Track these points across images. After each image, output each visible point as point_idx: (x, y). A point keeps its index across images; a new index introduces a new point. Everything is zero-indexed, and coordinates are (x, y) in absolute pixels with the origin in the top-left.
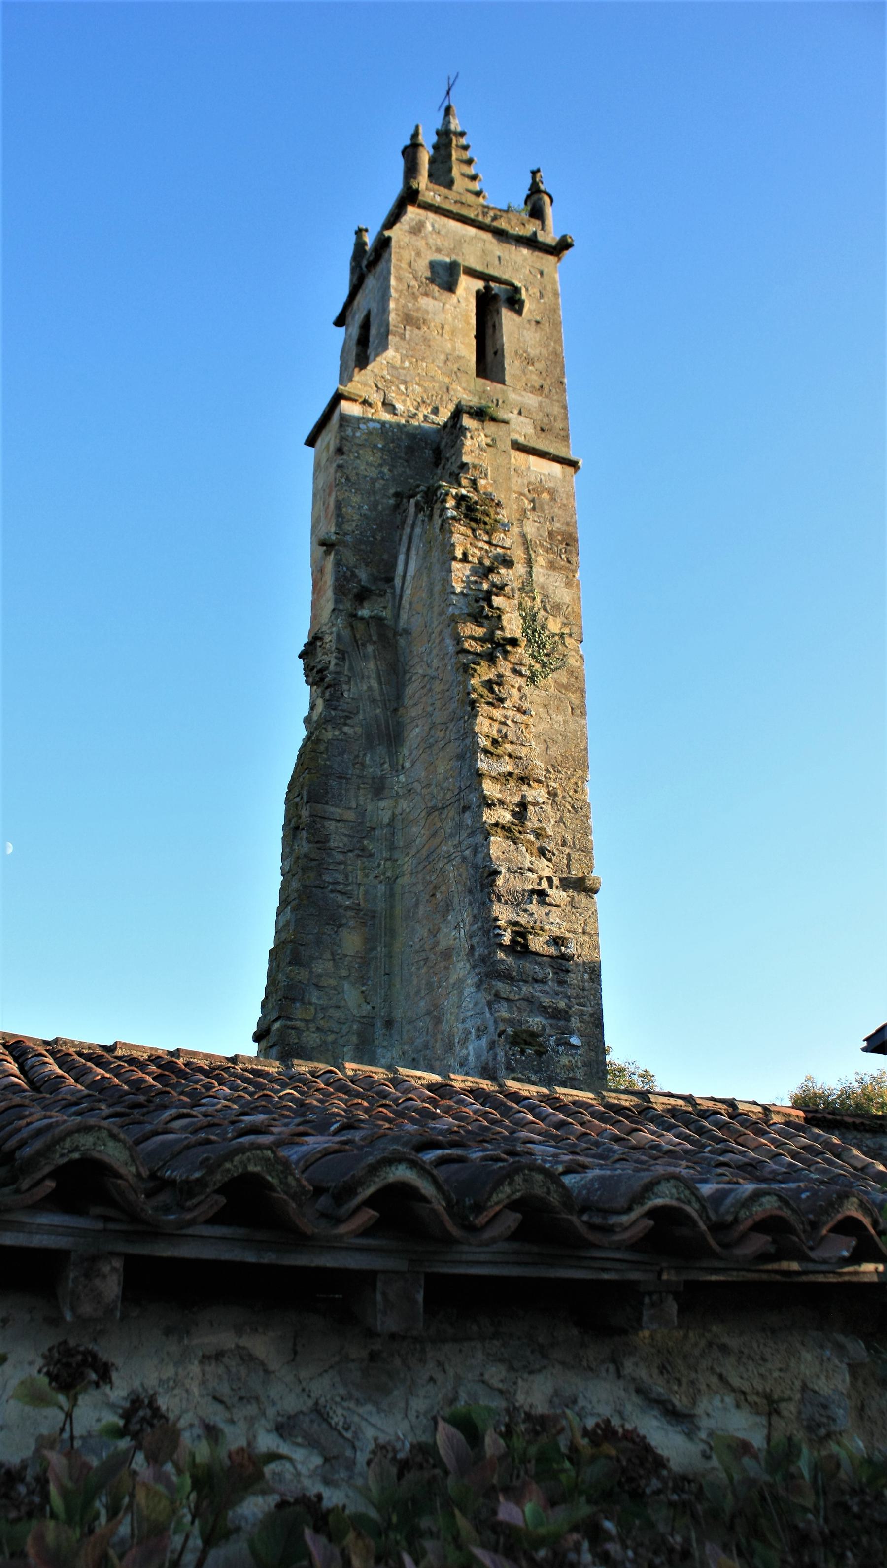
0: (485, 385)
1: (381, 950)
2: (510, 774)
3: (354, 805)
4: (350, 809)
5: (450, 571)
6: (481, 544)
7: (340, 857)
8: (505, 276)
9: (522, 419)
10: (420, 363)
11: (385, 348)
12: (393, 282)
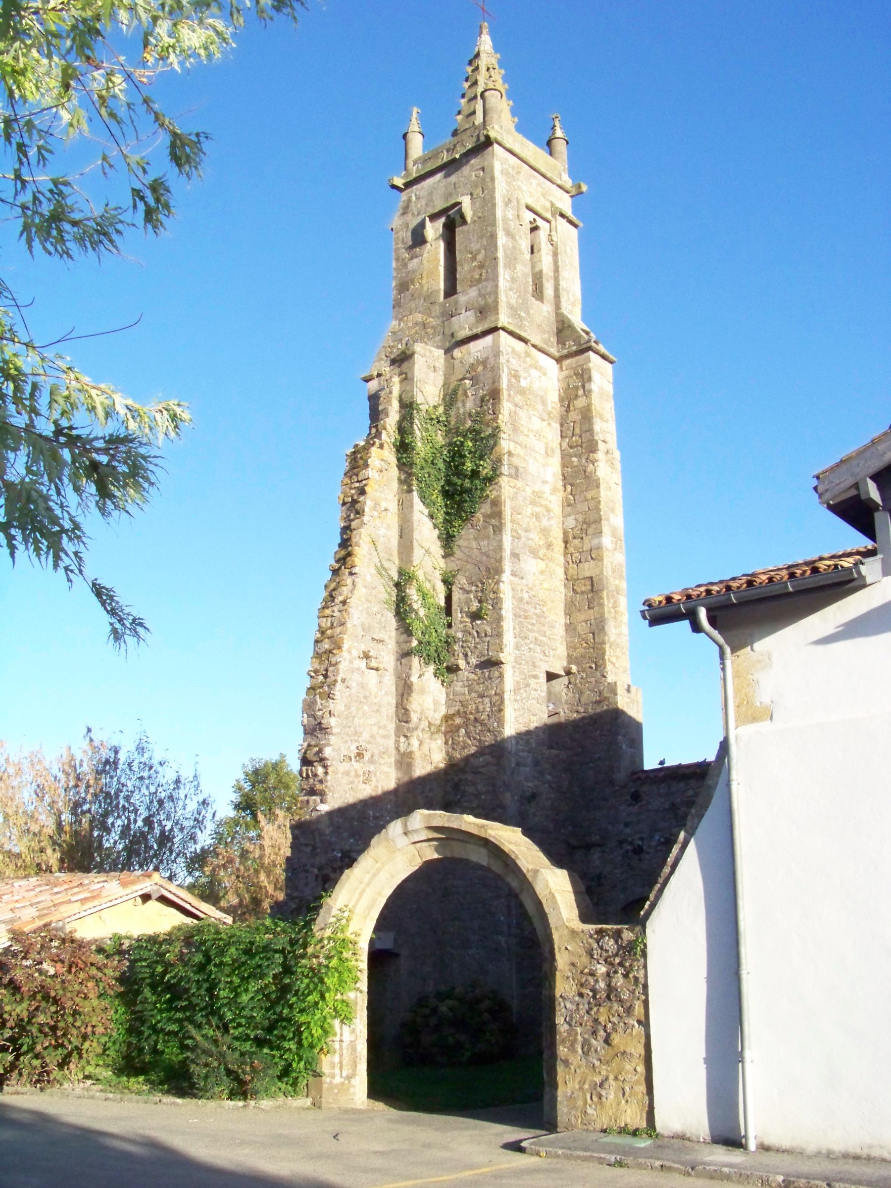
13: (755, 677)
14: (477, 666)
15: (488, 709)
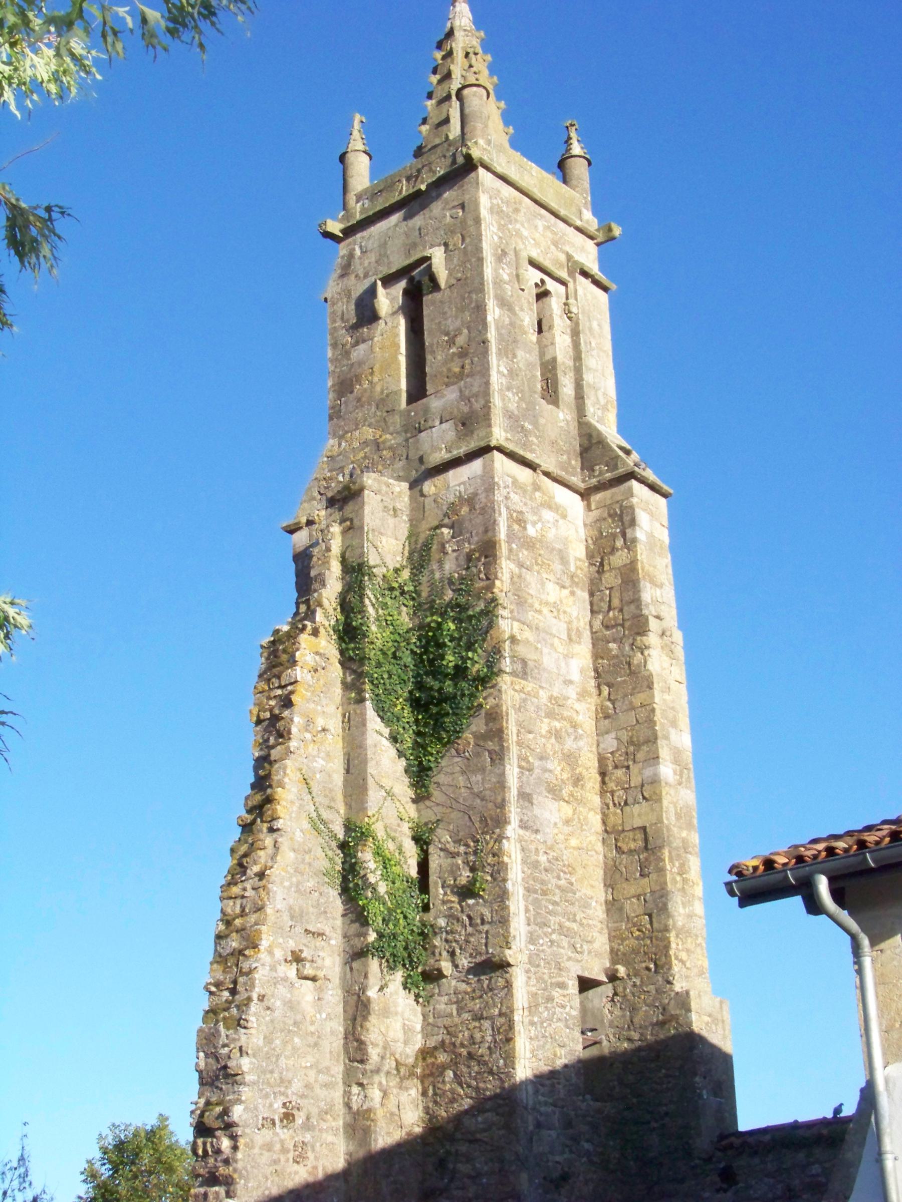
15: (489, 1039)
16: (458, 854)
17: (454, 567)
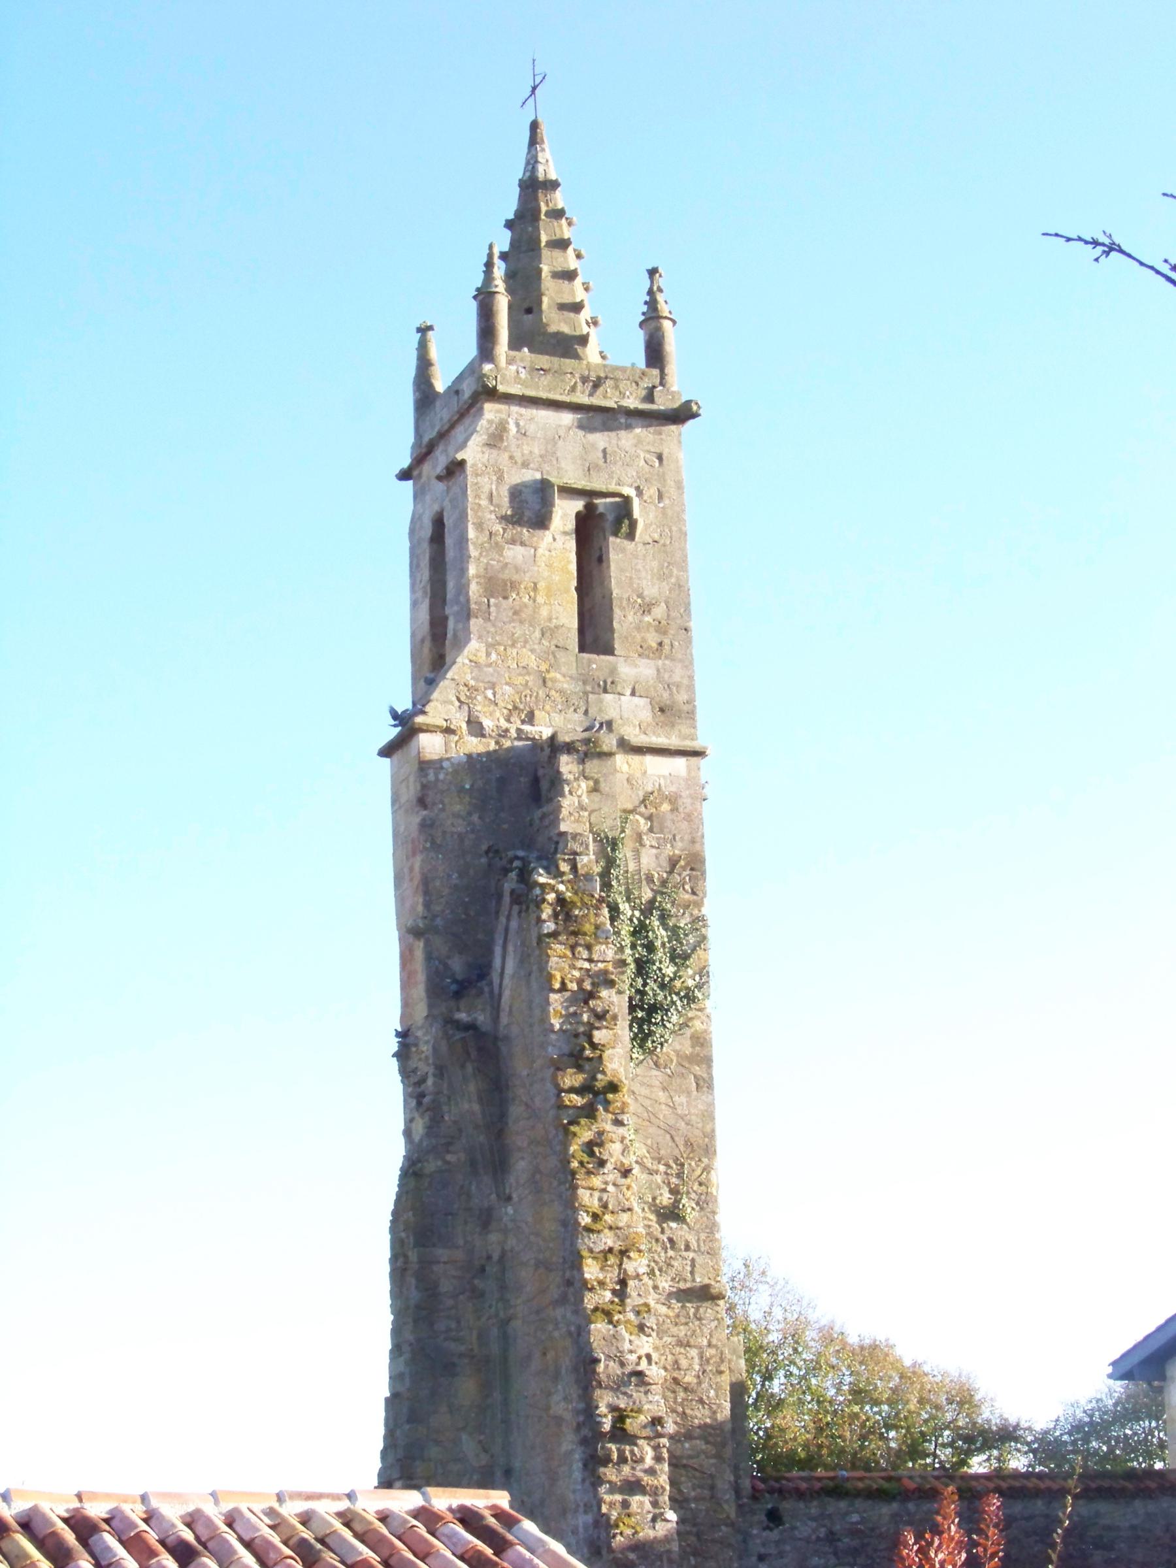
0: (590, 662)
1: (497, 1396)
2: (611, 1250)
3: (461, 1242)
4: (457, 1248)
5: (548, 1004)
6: (580, 964)
7: (451, 1302)
8: (613, 488)
9: (636, 700)
10: (509, 650)
11: (468, 640)
12: (471, 533)
13: (1119, 1386)
14: (670, 1295)
15: (697, 1367)
16: (657, 1172)
17: (653, 865)
